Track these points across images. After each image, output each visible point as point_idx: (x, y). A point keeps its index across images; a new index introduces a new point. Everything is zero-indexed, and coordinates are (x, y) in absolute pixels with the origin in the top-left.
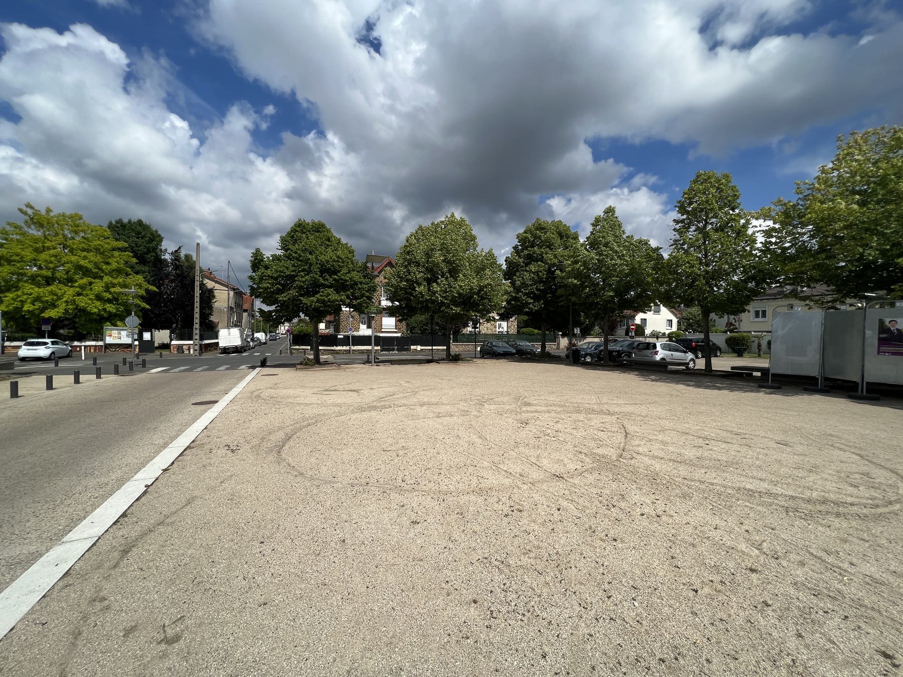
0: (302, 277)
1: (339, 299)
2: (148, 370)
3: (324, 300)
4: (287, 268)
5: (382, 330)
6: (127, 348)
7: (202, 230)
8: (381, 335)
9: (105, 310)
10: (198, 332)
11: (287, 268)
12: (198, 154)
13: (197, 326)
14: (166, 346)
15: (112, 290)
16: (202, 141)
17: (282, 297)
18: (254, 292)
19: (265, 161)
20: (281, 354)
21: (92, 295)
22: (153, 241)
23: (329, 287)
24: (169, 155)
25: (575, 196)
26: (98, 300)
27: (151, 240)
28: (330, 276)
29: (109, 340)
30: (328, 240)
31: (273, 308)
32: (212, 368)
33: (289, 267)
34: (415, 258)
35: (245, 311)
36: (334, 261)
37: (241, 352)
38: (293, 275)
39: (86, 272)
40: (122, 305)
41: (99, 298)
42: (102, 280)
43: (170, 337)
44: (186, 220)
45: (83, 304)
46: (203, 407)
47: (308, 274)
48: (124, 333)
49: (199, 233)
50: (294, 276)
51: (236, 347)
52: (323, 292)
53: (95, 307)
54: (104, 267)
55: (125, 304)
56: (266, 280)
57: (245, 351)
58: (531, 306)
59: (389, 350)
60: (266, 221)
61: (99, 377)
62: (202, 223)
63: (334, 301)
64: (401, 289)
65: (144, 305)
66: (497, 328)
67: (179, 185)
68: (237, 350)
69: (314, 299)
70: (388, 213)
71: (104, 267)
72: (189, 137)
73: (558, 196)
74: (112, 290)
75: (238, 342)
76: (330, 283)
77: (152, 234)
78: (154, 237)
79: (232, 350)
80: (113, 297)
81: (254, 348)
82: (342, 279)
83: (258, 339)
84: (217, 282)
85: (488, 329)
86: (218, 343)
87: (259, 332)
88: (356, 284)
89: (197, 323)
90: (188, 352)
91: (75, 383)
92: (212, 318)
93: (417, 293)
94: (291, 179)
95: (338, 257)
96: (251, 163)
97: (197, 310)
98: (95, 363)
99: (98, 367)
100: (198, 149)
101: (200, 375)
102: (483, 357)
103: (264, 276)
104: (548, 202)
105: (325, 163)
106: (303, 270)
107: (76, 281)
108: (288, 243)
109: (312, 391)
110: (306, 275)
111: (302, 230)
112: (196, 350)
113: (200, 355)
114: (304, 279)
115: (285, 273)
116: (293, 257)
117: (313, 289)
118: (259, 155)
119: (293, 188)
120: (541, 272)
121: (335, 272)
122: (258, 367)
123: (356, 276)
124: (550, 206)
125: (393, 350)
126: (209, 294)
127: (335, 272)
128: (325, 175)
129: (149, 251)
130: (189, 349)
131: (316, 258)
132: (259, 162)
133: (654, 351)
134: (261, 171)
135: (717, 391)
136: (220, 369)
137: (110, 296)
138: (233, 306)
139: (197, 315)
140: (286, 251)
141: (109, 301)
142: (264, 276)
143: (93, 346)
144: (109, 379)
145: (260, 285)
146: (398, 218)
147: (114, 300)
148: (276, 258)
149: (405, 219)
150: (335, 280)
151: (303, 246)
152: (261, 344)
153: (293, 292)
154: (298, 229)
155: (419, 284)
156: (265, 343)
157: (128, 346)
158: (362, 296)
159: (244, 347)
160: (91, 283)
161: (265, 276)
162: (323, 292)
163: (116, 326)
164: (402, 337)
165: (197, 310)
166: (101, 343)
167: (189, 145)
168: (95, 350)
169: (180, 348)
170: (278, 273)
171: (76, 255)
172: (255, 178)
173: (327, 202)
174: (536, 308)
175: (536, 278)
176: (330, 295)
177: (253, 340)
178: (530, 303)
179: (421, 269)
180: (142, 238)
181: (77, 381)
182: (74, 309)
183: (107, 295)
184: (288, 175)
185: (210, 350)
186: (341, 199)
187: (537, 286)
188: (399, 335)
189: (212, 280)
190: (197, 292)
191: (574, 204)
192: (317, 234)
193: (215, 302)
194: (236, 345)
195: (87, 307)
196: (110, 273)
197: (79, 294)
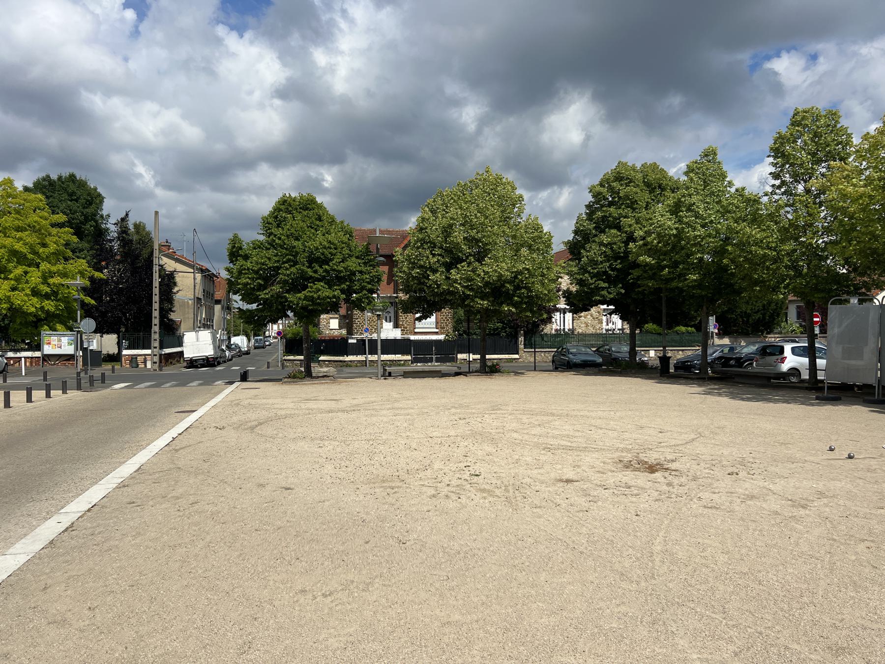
0: (287, 269)
1: (331, 295)
2: (111, 386)
3: (312, 296)
4: (269, 259)
5: (416, 330)
6: (68, 360)
7: (145, 164)
8: (412, 338)
9: (42, 308)
10: (157, 336)
11: (269, 259)
12: (136, 33)
13: (156, 328)
14: (114, 358)
15: (51, 281)
16: (141, 15)
17: (262, 295)
18: (232, 286)
19: (241, 36)
20: (268, 367)
21: (28, 290)
22: (91, 204)
23: (319, 280)
24: (93, 40)
25: (827, 48)
26: (33, 296)
27: (90, 203)
28: (321, 267)
29: (48, 350)
30: (320, 219)
31: (254, 306)
32: (183, 384)
33: (269, 258)
34: (429, 237)
35: (218, 302)
36: (325, 248)
37: (213, 365)
38: (277, 267)
39: (19, 258)
40: (62, 302)
41: (35, 293)
42: (38, 267)
43: (119, 344)
44: (119, 148)
45: (19, 302)
46: (186, 414)
47: (294, 266)
48: (65, 340)
49: (140, 169)
50: (279, 268)
51: (207, 359)
52: (311, 288)
53: (32, 305)
54: (41, 250)
55: (66, 300)
56: (246, 274)
57: (219, 363)
58: (604, 293)
59: (425, 361)
60: (243, 142)
61: (64, 392)
62: (144, 151)
63: (324, 298)
64: (414, 278)
65: (89, 300)
66: (604, 323)
67: (109, 90)
68: (208, 362)
69: (301, 295)
70: (453, 113)
71: (41, 250)
72: (122, 7)
73: (788, 51)
74: (51, 281)
75: (208, 351)
76: (320, 275)
77: (89, 194)
78: (92, 198)
79: (201, 362)
80: (52, 290)
81: (231, 360)
82: (334, 270)
83: (237, 346)
84: (177, 260)
85: (587, 326)
86: (182, 353)
87: (238, 335)
88: (353, 273)
89: (156, 325)
90: (143, 366)
91: (27, 402)
92: (173, 316)
93: (430, 282)
94: (285, 65)
95: (330, 242)
96: (219, 41)
97: (156, 306)
98: (45, 379)
99: (47, 383)
100: (136, 27)
101: (169, 390)
102: (556, 369)
103: (243, 270)
104: (768, 65)
105: (341, 30)
106: (288, 261)
107: (11, 272)
108: (270, 226)
109: (292, 400)
110: (291, 266)
111: (288, 209)
112: (156, 363)
113: (161, 370)
114: (288, 272)
115: (266, 265)
116: (276, 244)
117: (299, 284)
118: (232, 28)
119: (288, 79)
120: (615, 243)
121: (327, 261)
122: (238, 381)
123: (353, 264)
124: (776, 74)
125: (431, 360)
126: (169, 280)
127: (327, 261)
128: (342, 53)
129: (87, 219)
130: (145, 362)
131: (303, 244)
132: (232, 41)
133: (780, 357)
134: (234, 55)
135: (771, 405)
136: (191, 384)
137: (48, 290)
138: (201, 296)
139: (156, 314)
140: (269, 237)
141: (47, 296)
142: (243, 270)
143: (28, 358)
144: (73, 394)
145: (239, 281)
146: (470, 121)
147: (53, 295)
148: (257, 246)
149: (483, 122)
150: (326, 271)
151: (289, 230)
152: (241, 354)
153: (277, 288)
154: (282, 207)
155: (435, 271)
156: (247, 353)
157: (70, 358)
158: (363, 288)
159: (217, 358)
160: (26, 273)
161: (245, 269)
162: (311, 288)
163: (55, 330)
164: (445, 341)
165: (156, 306)
166: (38, 354)
167: (122, 20)
168: (31, 363)
169: (133, 359)
170: (259, 266)
171: (9, 237)
172: (228, 68)
173: (345, 101)
174: (612, 296)
175: (609, 252)
176: (319, 290)
177: (229, 347)
178: (603, 289)
179: (437, 251)
180: (76, 200)
181: (48, 395)
182: (9, 309)
183: (45, 289)
184: (281, 58)
185: (171, 363)
186: (369, 94)
187: (611, 264)
188: (441, 337)
189: (170, 257)
190: (156, 281)
191: (823, 66)
192: (305, 213)
193: (178, 292)
194: (207, 354)
195: (23, 306)
196: (47, 259)
197: (13, 289)
